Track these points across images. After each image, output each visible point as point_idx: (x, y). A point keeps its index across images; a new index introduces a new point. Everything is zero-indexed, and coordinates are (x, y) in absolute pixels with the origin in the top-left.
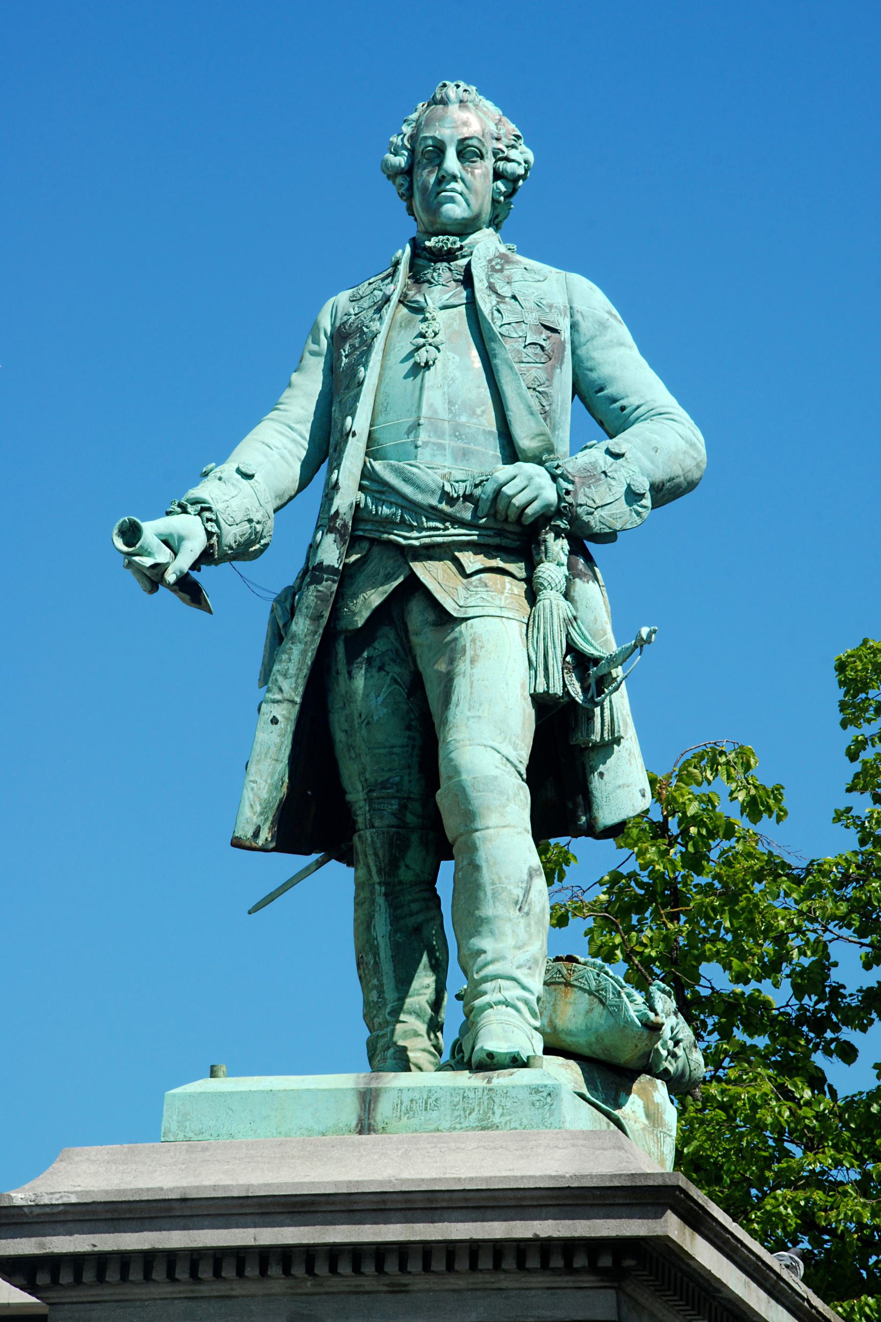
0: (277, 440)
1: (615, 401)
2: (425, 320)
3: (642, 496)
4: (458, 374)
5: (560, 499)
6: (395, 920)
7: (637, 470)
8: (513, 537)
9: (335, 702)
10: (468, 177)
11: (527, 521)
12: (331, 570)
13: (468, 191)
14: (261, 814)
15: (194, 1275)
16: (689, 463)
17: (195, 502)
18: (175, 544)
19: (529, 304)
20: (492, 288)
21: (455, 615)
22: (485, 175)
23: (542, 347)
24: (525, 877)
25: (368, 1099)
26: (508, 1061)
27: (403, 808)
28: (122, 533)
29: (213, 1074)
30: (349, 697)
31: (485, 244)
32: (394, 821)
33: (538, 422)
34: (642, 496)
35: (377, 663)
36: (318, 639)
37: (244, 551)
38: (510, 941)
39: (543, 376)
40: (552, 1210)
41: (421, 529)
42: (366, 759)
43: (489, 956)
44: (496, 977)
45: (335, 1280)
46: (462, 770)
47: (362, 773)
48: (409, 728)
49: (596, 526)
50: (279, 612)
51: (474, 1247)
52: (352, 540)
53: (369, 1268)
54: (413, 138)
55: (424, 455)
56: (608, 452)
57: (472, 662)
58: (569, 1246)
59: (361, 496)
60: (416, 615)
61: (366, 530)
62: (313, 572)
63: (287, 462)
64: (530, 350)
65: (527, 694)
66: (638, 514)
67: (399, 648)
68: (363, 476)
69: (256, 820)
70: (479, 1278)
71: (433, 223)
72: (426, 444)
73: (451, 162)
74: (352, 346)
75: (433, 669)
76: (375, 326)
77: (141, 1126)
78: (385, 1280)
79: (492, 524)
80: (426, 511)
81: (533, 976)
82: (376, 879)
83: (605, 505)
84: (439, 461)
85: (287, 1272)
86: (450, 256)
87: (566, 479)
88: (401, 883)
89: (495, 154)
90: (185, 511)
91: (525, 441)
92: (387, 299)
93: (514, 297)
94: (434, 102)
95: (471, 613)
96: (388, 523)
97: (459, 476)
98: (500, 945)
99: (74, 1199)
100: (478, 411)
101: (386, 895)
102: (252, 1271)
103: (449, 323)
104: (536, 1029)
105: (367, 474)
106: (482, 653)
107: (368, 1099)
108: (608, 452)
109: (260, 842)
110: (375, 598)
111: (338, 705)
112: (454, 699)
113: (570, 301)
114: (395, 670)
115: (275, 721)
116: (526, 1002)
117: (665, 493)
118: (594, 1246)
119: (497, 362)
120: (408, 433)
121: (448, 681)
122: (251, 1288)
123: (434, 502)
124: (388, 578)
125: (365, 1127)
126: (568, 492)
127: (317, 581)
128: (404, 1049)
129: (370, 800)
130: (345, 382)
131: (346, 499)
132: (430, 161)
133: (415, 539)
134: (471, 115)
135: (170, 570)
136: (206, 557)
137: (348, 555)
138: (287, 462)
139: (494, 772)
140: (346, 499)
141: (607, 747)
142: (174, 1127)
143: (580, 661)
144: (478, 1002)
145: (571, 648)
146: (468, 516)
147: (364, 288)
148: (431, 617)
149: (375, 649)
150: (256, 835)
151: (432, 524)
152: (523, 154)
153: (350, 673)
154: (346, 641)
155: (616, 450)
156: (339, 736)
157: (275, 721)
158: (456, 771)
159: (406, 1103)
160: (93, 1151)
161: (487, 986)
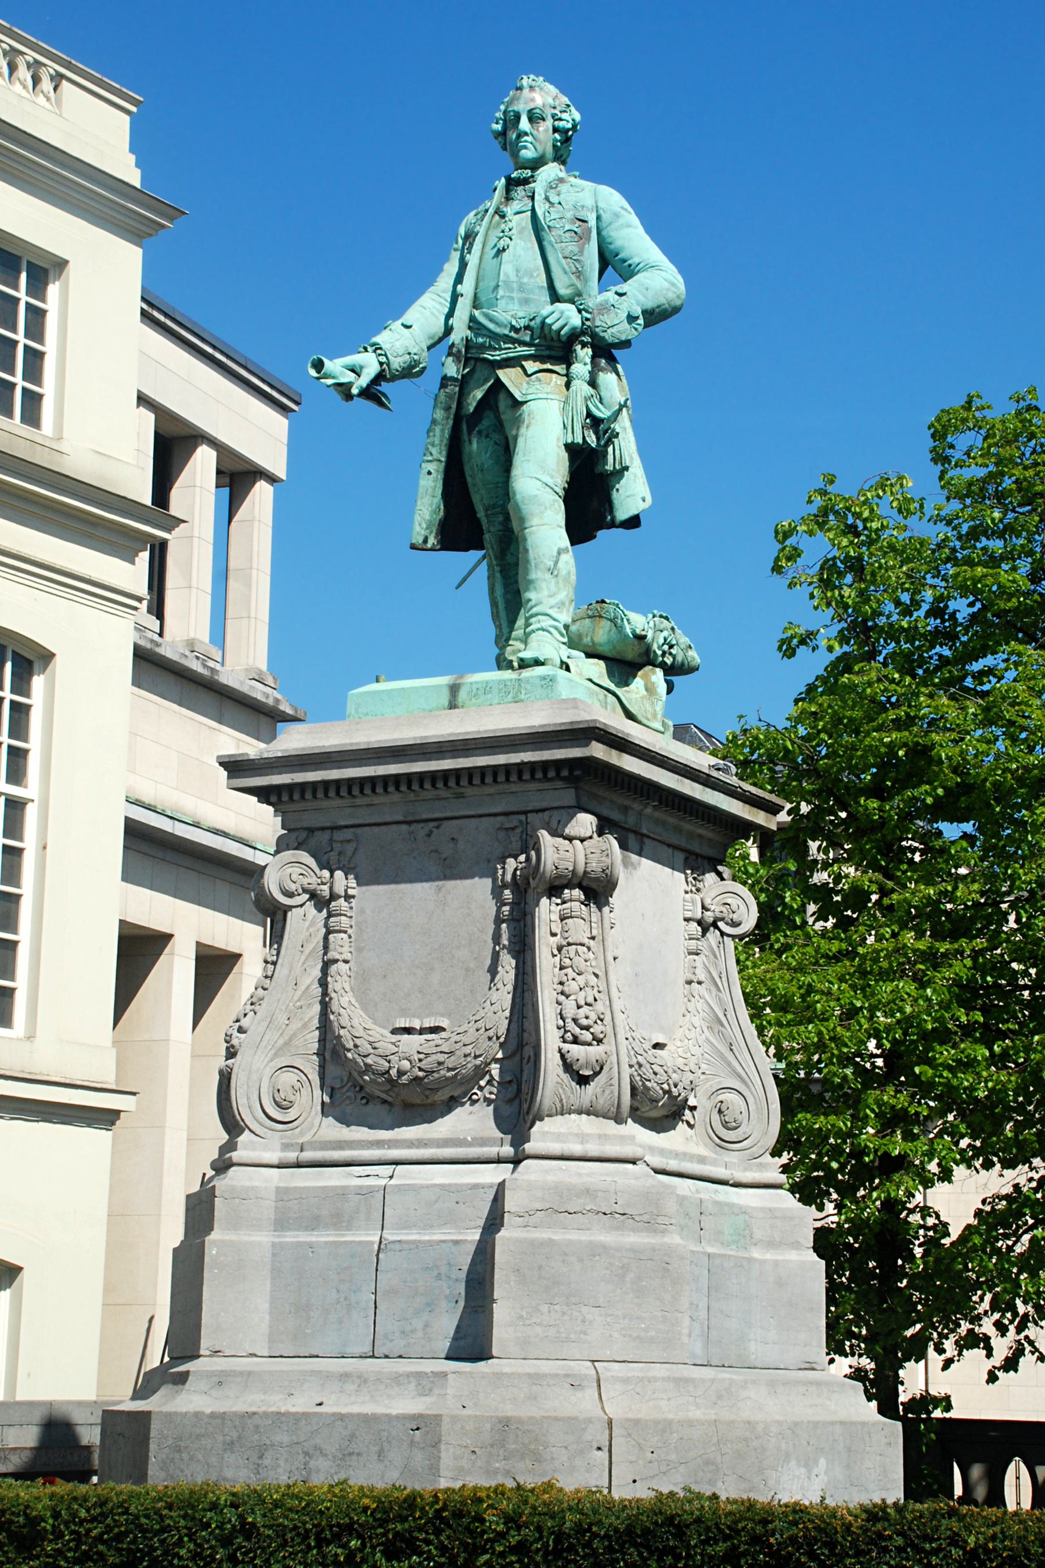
1: (625, 261)
3: (637, 318)
4: (522, 253)
5: (583, 324)
7: (634, 302)
8: (555, 349)
10: (535, 132)
11: (564, 339)
12: (452, 379)
13: (536, 140)
14: (427, 529)
16: (671, 295)
18: (358, 370)
20: (547, 199)
21: (520, 399)
22: (546, 131)
23: (576, 233)
24: (555, 554)
25: (454, 689)
26: (532, 662)
29: (377, 681)
30: (470, 453)
31: (551, 171)
32: (501, 528)
33: (570, 278)
34: (637, 318)
35: (484, 433)
36: (451, 422)
37: (410, 372)
38: (546, 593)
39: (576, 250)
40: (531, 746)
41: (501, 349)
42: (483, 491)
44: (537, 615)
45: (424, 793)
46: (517, 492)
47: (482, 500)
49: (610, 340)
51: (495, 769)
53: (440, 784)
54: (505, 112)
55: (502, 304)
56: (616, 293)
57: (527, 427)
59: (469, 332)
60: (503, 403)
61: (473, 353)
63: (435, 316)
64: (568, 235)
65: (561, 444)
66: (636, 329)
72: (502, 297)
73: (524, 124)
77: (337, 712)
79: (543, 343)
81: (561, 612)
82: (494, 562)
83: (615, 326)
84: (511, 306)
87: (587, 311)
88: (509, 564)
89: (553, 117)
93: (560, 203)
95: (529, 398)
96: (483, 348)
97: (521, 314)
98: (540, 596)
99: (280, 755)
100: (535, 274)
101: (501, 572)
103: (518, 221)
104: (564, 643)
105: (472, 319)
106: (533, 422)
107: (454, 689)
109: (429, 545)
110: (479, 394)
113: (596, 203)
114: (496, 436)
115: (429, 473)
116: (556, 628)
117: (654, 316)
119: (545, 243)
120: (493, 291)
121: (516, 438)
123: (506, 332)
124: (486, 381)
125: (453, 705)
126: (587, 319)
129: (487, 516)
133: (497, 356)
135: (354, 387)
138: (435, 316)
139: (535, 492)
142: (353, 713)
143: (595, 422)
146: (527, 339)
150: (426, 541)
151: (507, 346)
153: (470, 441)
155: (621, 291)
156: (469, 479)
159: (475, 690)
161: (532, 620)
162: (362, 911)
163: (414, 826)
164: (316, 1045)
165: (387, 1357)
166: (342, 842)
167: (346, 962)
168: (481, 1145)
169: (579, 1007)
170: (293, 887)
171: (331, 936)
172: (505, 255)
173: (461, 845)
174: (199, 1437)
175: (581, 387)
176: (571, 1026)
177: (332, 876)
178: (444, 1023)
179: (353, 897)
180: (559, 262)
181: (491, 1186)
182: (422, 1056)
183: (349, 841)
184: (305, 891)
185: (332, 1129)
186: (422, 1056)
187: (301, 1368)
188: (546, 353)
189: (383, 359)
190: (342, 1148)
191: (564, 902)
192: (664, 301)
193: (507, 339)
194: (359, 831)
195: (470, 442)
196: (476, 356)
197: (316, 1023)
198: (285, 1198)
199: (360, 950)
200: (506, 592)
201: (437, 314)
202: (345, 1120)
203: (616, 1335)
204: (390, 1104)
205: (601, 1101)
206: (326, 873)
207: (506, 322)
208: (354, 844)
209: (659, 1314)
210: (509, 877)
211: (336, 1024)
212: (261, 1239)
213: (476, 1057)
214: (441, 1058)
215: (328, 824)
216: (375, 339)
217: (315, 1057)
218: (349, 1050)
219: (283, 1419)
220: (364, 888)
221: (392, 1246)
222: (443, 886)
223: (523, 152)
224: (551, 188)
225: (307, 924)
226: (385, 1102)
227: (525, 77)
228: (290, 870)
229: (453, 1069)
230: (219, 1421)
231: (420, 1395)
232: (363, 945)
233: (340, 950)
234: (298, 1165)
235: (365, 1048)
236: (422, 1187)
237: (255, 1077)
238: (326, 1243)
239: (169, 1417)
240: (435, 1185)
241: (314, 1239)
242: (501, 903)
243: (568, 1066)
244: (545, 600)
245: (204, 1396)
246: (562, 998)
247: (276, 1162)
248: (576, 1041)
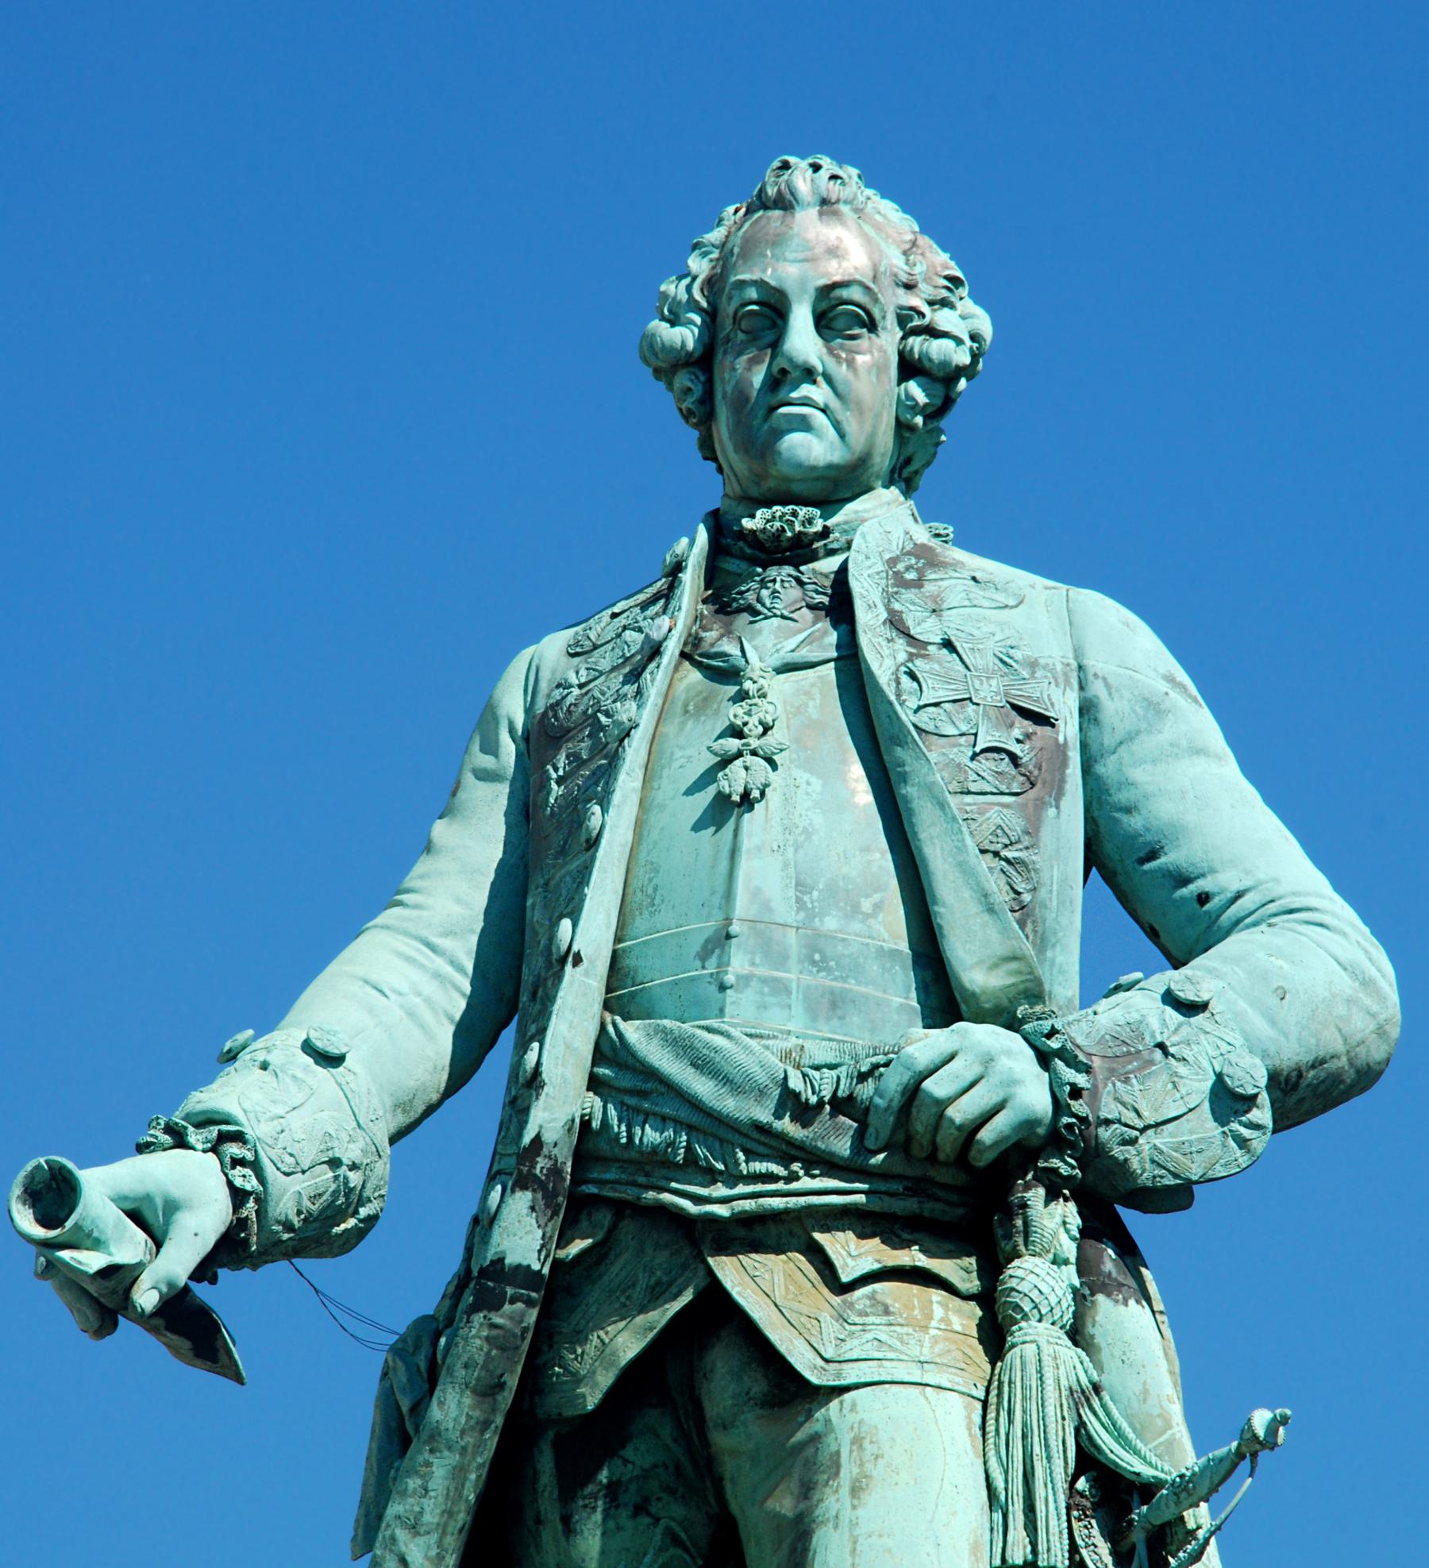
0: (397, 975)
1: (1184, 880)
2: (742, 696)
3: (1250, 1101)
4: (818, 819)
5: (1058, 1107)
7: (1237, 1039)
8: (947, 1195)
10: (841, 372)
11: (982, 1160)
12: (523, 1276)
13: (847, 397)
16: (1360, 1025)
17: (204, 1121)
18: (156, 1219)
20: (896, 623)
21: (815, 1380)
22: (880, 368)
23: (1014, 759)
28: (33, 1196)
33: (1005, 930)
34: (1250, 1101)
35: (631, 1496)
36: (491, 1440)
37: (324, 1233)
39: (1015, 824)
50: (401, 1376)
54: (713, 284)
55: (741, 1007)
57: (855, 1491)
60: (724, 1383)
61: (607, 1181)
62: (481, 1281)
63: (422, 1026)
64: (986, 765)
66: (1243, 1143)
67: (685, 1461)
71: (759, 477)
72: (745, 980)
73: (802, 338)
74: (573, 757)
76: (626, 711)
79: (900, 1168)
80: (746, 1136)
83: (1165, 1122)
84: (774, 1019)
86: (798, 550)
89: (902, 320)
90: (181, 1143)
91: (976, 970)
92: (654, 651)
93: (948, 644)
94: (762, 203)
100: (866, 905)
103: (797, 702)
105: (608, 1050)
106: (877, 1471)
110: (627, 1340)
113: (1078, 652)
114: (674, 1512)
117: (1305, 1094)
120: (704, 955)
123: (764, 1115)
124: (657, 1295)
126: (1076, 1093)
127: (490, 1302)
130: (557, 839)
131: (554, 1115)
132: (753, 336)
133: (720, 1201)
134: (848, 234)
135: (146, 1280)
137: (563, 1241)
140: (554, 1115)
145: (1088, 1460)
146: (842, 1146)
147: (601, 626)
148: (758, 1385)
149: (626, 1462)
152: (966, 320)
153: (566, 1520)
154: (558, 1446)
155: (1188, 994)
172: (752, 822)
175: (1039, 1341)
180: (964, 869)
188: (899, 1206)
189: (245, 1179)
192: (1339, 1047)
195: (568, 1527)
196: (628, 1194)
201: (428, 1017)
207: (762, 1078)
216: (205, 1099)
224: (901, 582)
227: (800, 164)
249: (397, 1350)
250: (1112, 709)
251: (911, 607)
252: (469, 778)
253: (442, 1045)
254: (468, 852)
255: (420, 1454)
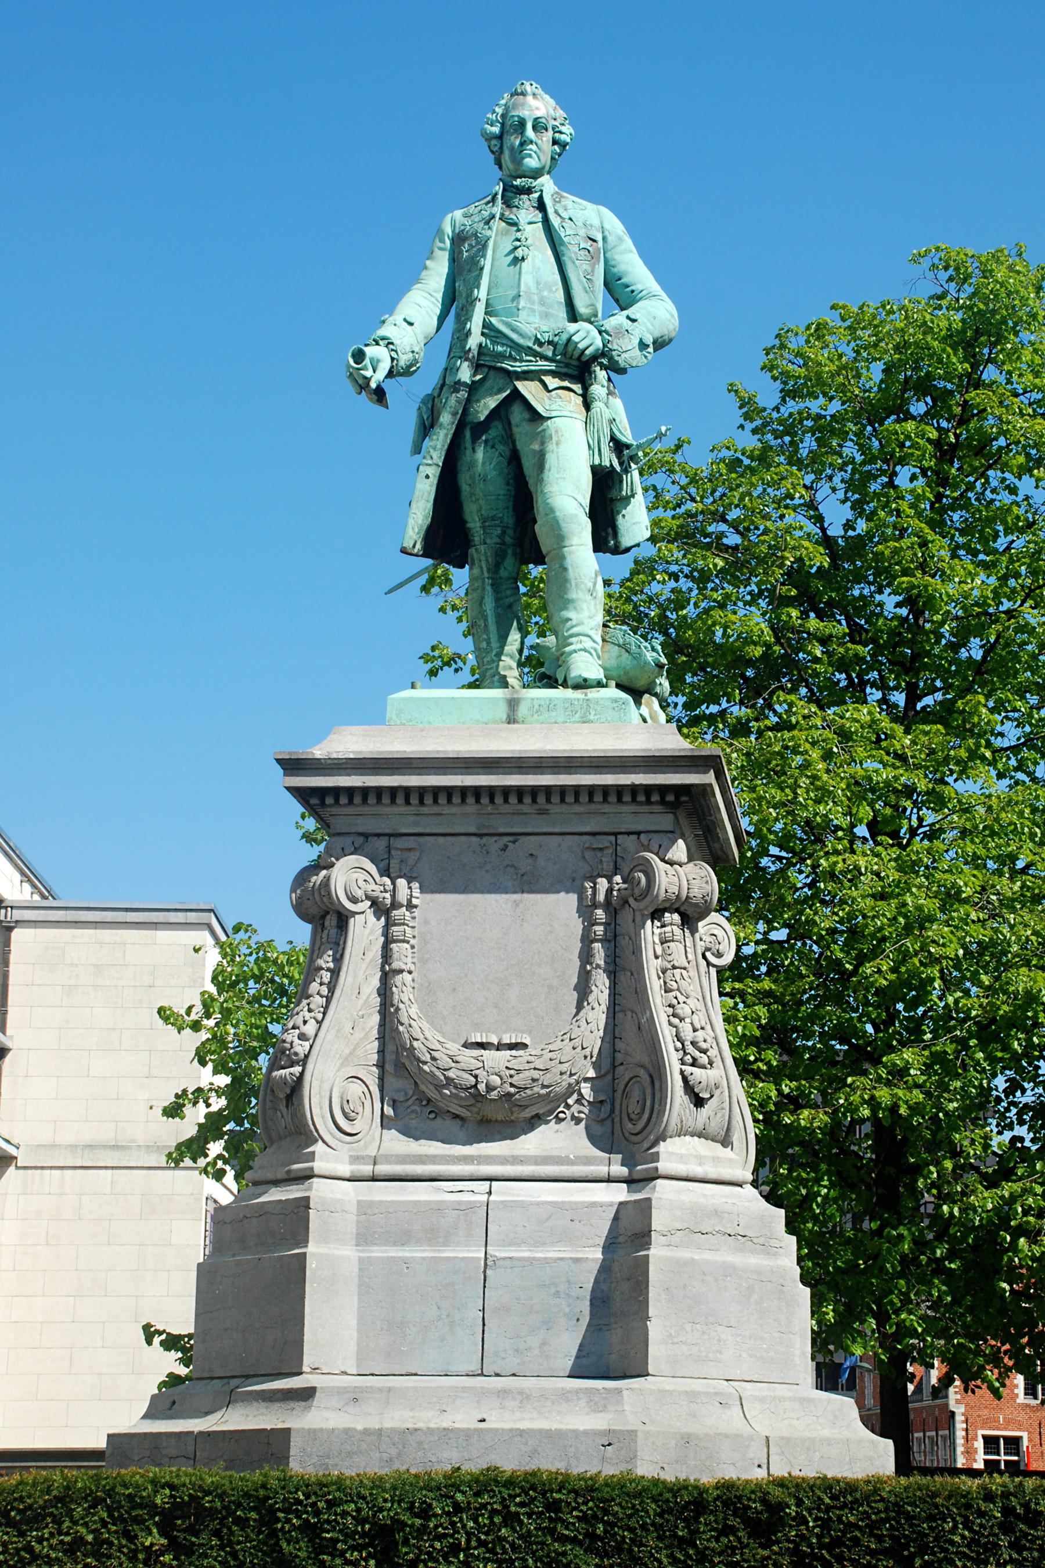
0: (424, 303)
2: (519, 230)
6: (497, 600)
8: (577, 369)
9: (463, 466)
10: (539, 142)
11: (584, 359)
12: (465, 384)
15: (422, 802)
17: (383, 339)
19: (580, 224)
20: (556, 212)
27: (504, 532)
28: (353, 356)
29: (413, 686)
30: (472, 464)
35: (490, 443)
37: (407, 372)
38: (586, 614)
39: (589, 269)
41: (521, 361)
42: (482, 502)
43: (574, 622)
48: (508, 484)
50: (424, 409)
52: (477, 367)
53: (528, 800)
54: (503, 115)
55: (523, 315)
56: (628, 317)
58: (648, 789)
60: (517, 414)
61: (486, 360)
62: (447, 384)
64: (582, 252)
68: (484, 327)
69: (415, 537)
70: (593, 806)
71: (516, 170)
73: (530, 132)
74: (470, 245)
75: (527, 449)
76: (488, 233)
77: (374, 715)
78: (536, 807)
82: (486, 575)
83: (627, 352)
84: (532, 319)
85: (478, 801)
86: (529, 191)
90: (377, 344)
91: (582, 309)
92: (493, 217)
94: (516, 93)
95: (553, 414)
96: (501, 356)
99: (352, 756)
102: (456, 800)
103: (534, 233)
105: (486, 325)
108: (628, 317)
111: (464, 468)
112: (547, 466)
114: (501, 448)
115: (427, 477)
117: (660, 344)
118: (663, 789)
119: (565, 259)
120: (513, 300)
122: (454, 810)
123: (530, 344)
124: (500, 391)
125: (511, 720)
127: (457, 391)
128: (505, 677)
129: (484, 527)
130: (467, 267)
131: (474, 341)
132: (516, 131)
133: (518, 367)
134: (538, 105)
136: (390, 374)
137: (474, 375)
140: (474, 341)
141: (627, 500)
142: (394, 717)
143: (619, 447)
144: (567, 649)
145: (613, 438)
146: (550, 354)
147: (472, 209)
148: (527, 415)
152: (567, 129)
155: (633, 317)
156: (465, 488)
157: (427, 477)
158: (552, 510)
160: (354, 729)
161: (573, 640)
162: (426, 922)
163: (485, 839)
164: (376, 1056)
165: (497, 1375)
166: (402, 850)
167: (410, 972)
168: (585, 1164)
169: (695, 1030)
170: (359, 894)
171: (393, 946)
172: (524, 264)
173: (541, 862)
174: (350, 1454)
175: (598, 406)
176: (690, 1049)
177: (394, 883)
178: (527, 1041)
179: (416, 907)
181: (611, 1205)
182: (512, 1072)
183: (410, 850)
184: (368, 897)
185: (396, 1142)
186: (512, 1072)
187: (433, 1385)
190: (423, 1163)
191: (663, 926)
193: (530, 351)
194: (422, 839)
197: (375, 1033)
198: (369, 1211)
199: (421, 960)
200: (497, 607)
202: (408, 1132)
203: (744, 1355)
204: (462, 1119)
205: (713, 1124)
206: (387, 881)
208: (417, 854)
209: (777, 1335)
210: (601, 897)
211: (407, 1036)
212: (348, 1253)
213: (571, 1075)
214: (536, 1074)
215: (387, 831)
217: (374, 1069)
218: (425, 1063)
219: (451, 1435)
220: (428, 897)
221: (501, 1262)
222: (521, 901)
223: (527, 160)
225: (367, 931)
226: (456, 1116)
228: (355, 875)
229: (547, 1087)
230: (374, 1438)
231: (594, 1411)
232: (427, 956)
233: (405, 960)
234: (374, 1179)
235: (444, 1061)
236: (531, 1204)
237: (327, 1087)
238: (424, 1258)
239: (313, 1434)
240: (546, 1203)
241: (407, 1254)
242: (590, 922)
243: (689, 1088)
244: (586, 621)
245: (341, 1414)
246: (676, 1021)
247: (347, 1175)
248: (694, 1064)
249: (423, 402)
250: (610, 238)
251: (558, 207)
252: (436, 250)
253: (435, 323)
254: (438, 270)
255: (436, 429)
